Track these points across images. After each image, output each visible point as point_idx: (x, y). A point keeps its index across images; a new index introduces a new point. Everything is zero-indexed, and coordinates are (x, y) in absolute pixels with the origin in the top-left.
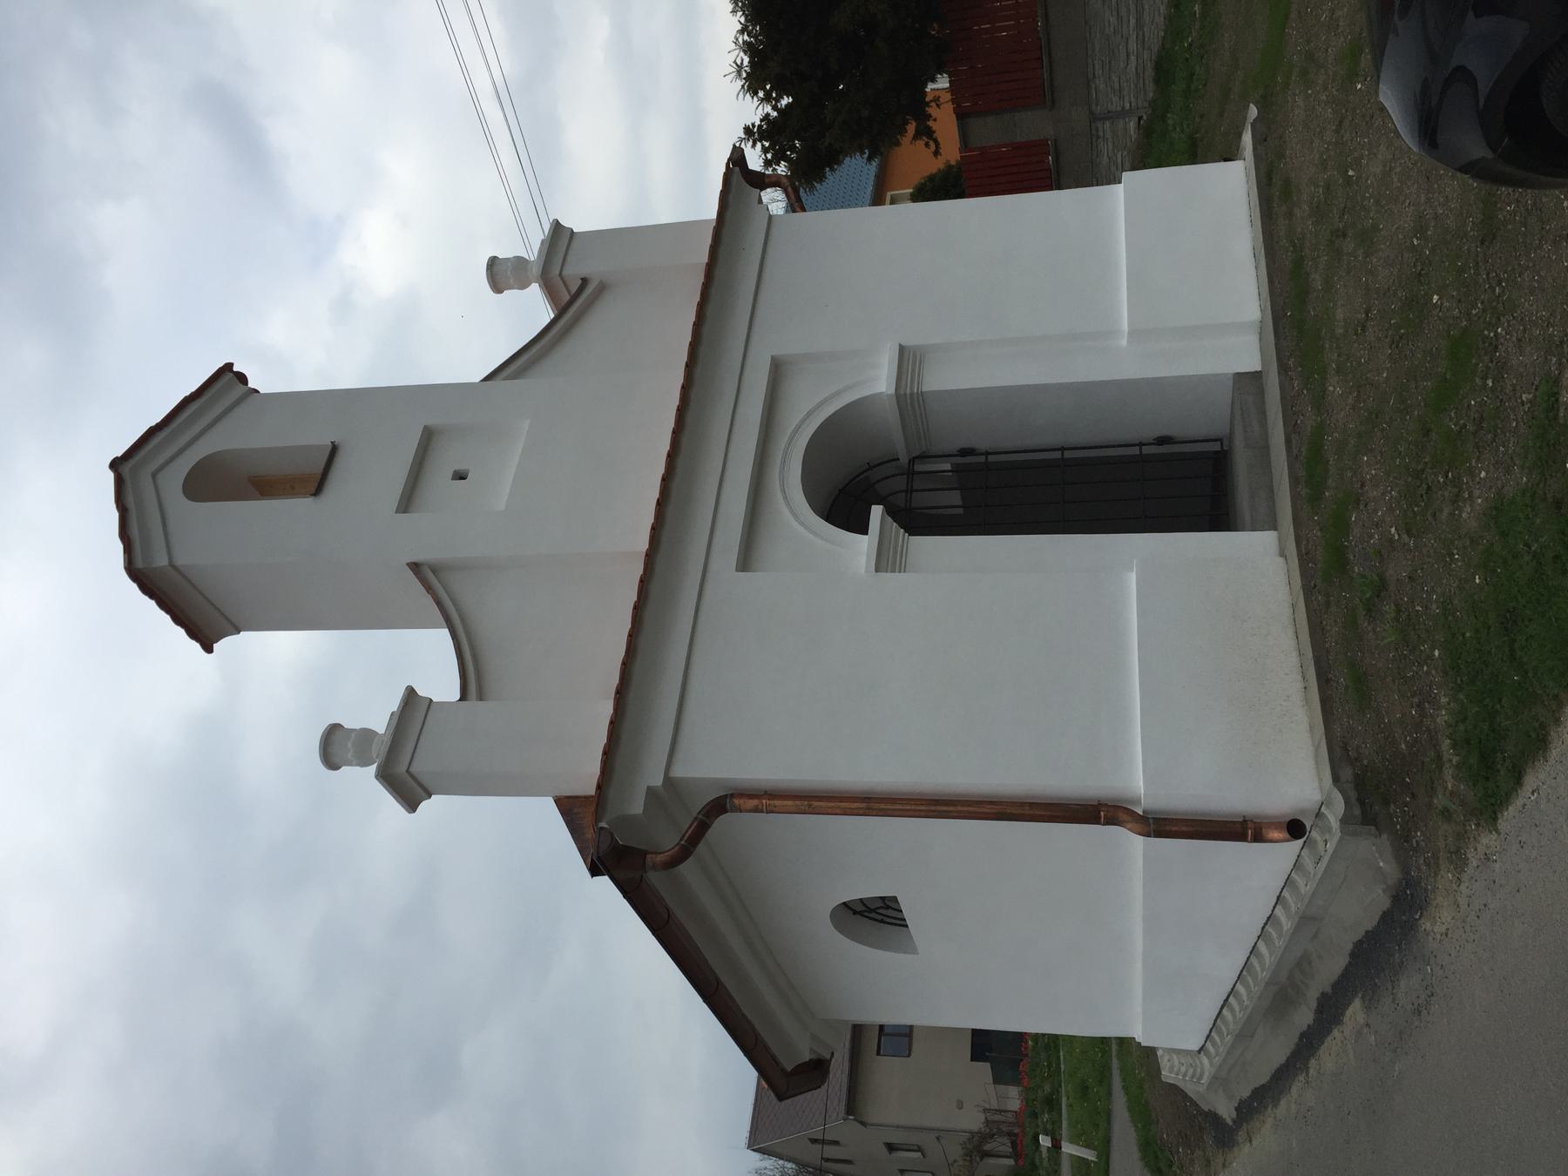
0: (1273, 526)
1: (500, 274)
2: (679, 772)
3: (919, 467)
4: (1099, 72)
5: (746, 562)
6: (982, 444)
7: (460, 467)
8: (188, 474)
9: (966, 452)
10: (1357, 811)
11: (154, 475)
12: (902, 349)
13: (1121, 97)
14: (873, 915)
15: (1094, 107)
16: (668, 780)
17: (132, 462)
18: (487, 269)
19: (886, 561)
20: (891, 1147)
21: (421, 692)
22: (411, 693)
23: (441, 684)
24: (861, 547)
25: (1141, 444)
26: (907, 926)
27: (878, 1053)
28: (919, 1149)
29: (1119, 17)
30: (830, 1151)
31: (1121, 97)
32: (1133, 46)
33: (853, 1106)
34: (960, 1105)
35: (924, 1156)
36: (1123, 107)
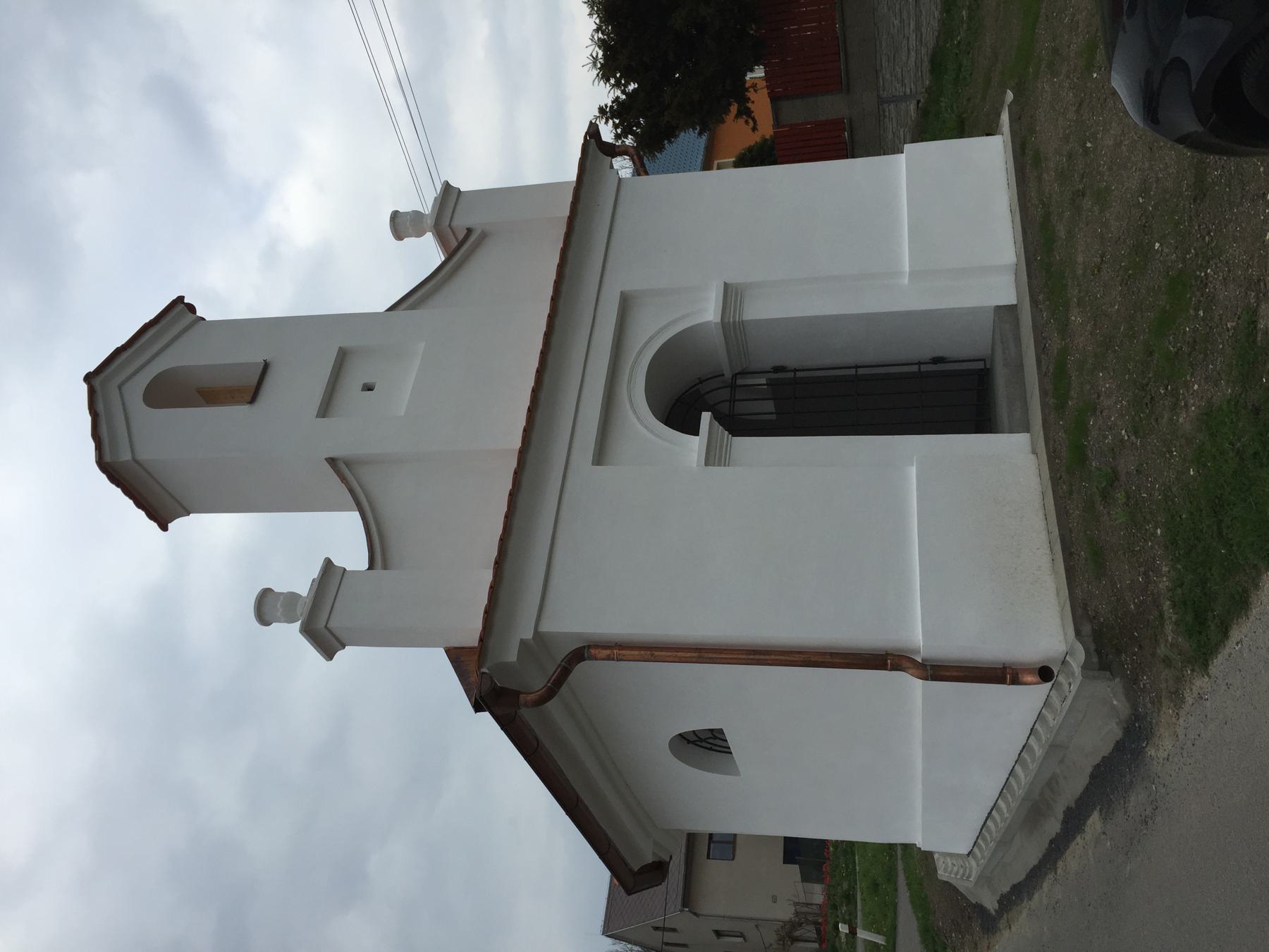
0: (1026, 429)
1: (401, 225)
2: (547, 627)
3: (740, 382)
4: (885, 64)
5: (600, 457)
6: (791, 363)
7: (368, 380)
8: (148, 385)
9: (778, 369)
10: (1095, 660)
11: (120, 387)
12: (726, 285)
13: (903, 85)
14: (704, 744)
15: (881, 92)
16: (536, 633)
17: (102, 376)
18: (391, 221)
19: (713, 457)
20: (718, 934)
21: (336, 562)
22: (328, 564)
23: (353, 556)
24: (693, 446)
25: (919, 363)
26: (731, 753)
27: (708, 857)
28: (742, 935)
29: (902, 21)
30: (670, 937)
31: (903, 85)
32: (913, 42)
33: (687, 900)
34: (775, 900)
35: (744, 939)
36: (905, 93)
